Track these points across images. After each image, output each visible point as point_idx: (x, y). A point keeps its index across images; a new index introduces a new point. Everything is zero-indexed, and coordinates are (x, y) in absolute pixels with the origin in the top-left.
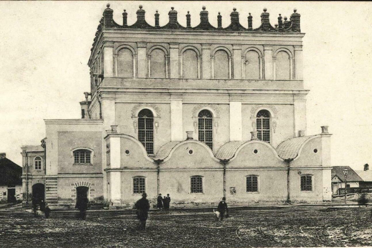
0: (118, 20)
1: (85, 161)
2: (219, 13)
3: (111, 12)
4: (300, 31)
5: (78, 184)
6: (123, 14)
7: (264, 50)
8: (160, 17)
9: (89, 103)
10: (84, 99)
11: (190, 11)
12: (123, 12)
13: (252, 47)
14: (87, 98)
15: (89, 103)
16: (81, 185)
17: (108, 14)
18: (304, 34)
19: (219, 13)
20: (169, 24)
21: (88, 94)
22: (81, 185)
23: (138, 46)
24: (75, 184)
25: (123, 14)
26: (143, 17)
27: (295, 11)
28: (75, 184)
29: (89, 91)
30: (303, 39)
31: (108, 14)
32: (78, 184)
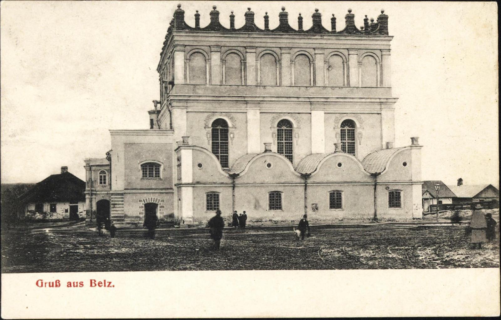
1: (154, 175)
4: (387, 33)
5: (147, 200)
6: (196, 15)
7: (349, 55)
9: (159, 112)
10: (153, 108)
11: (268, 12)
13: (336, 51)
14: (156, 106)
15: (159, 112)
16: (149, 201)
17: (179, 15)
18: (393, 37)
19: (300, 14)
21: (158, 103)
23: (212, 50)
24: (143, 200)
25: (196, 15)
27: (382, 12)
28: (143, 200)
29: (158, 99)
30: (391, 43)
31: (179, 15)
32: (147, 200)
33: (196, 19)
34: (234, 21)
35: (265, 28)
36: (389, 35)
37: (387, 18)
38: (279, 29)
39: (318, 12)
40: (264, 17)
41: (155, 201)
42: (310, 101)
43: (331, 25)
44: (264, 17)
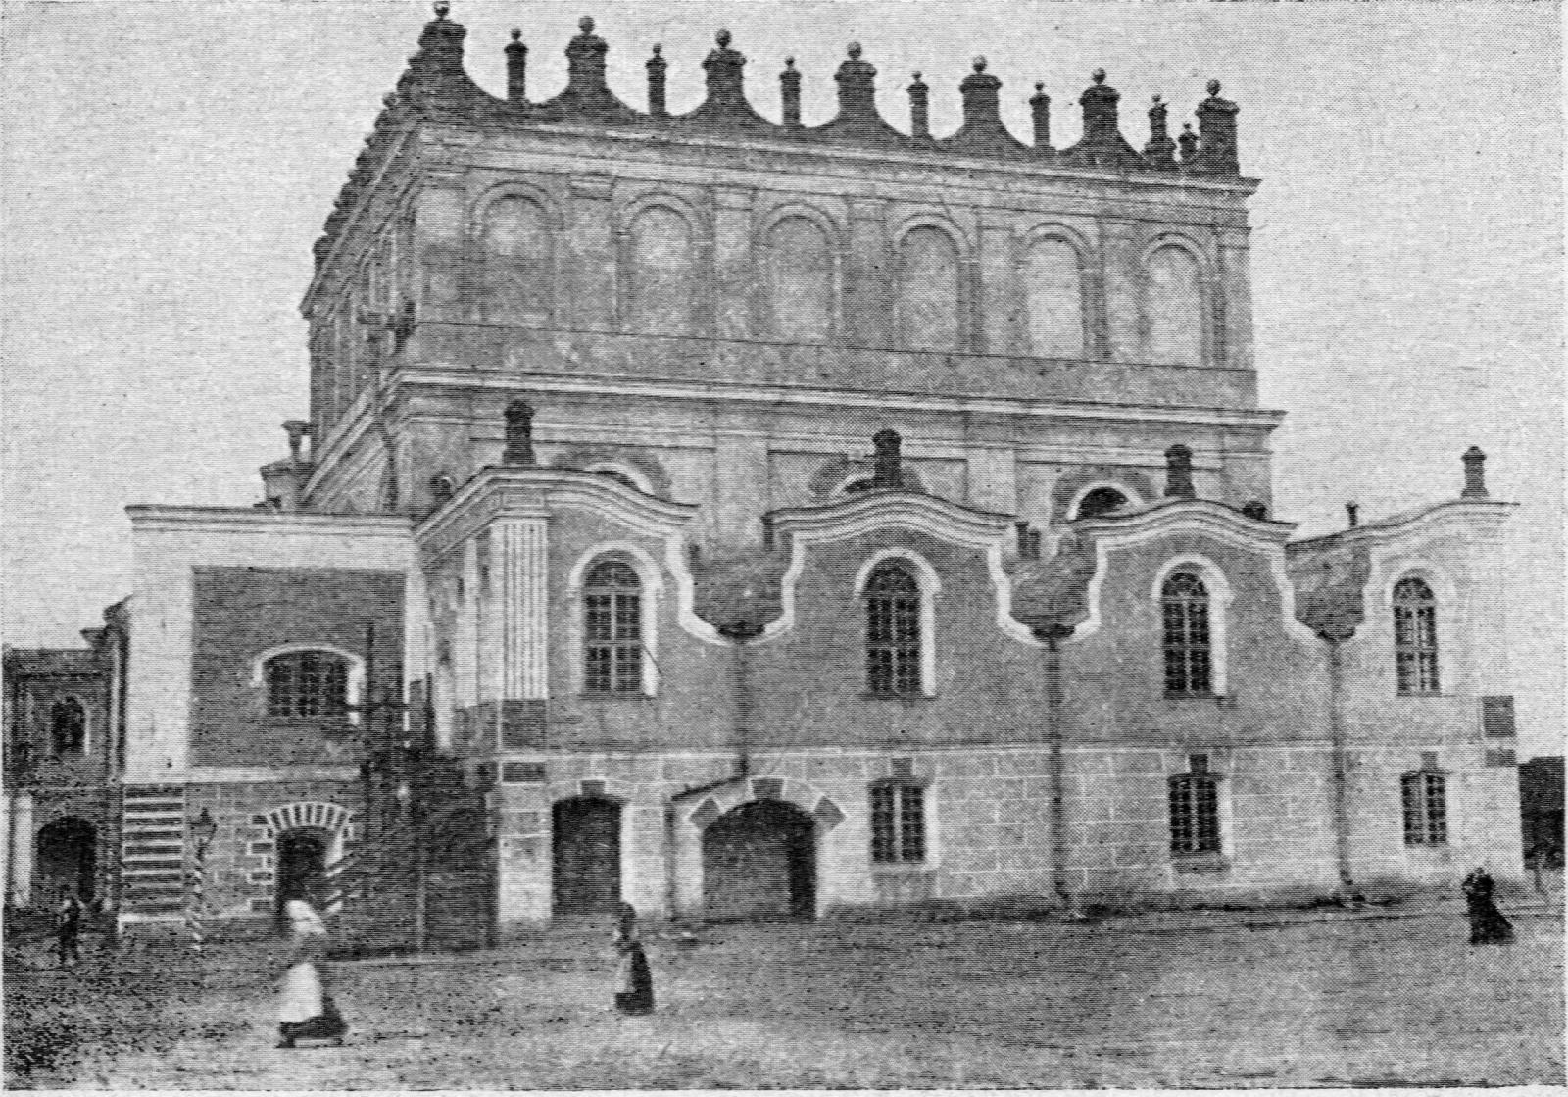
0: (486, 71)
1: (614, 681)
2: (516, 35)
3: (1112, 98)
4: (1235, 167)
5: (287, 818)
6: (784, 77)
7: (980, 229)
8: (671, 73)
9: (308, 469)
10: (282, 452)
11: (797, 57)
12: (784, 68)
13: (1053, 223)
14: (295, 445)
15: (308, 469)
16: (288, 823)
17: (443, 40)
18: (1256, 182)
19: (516, 35)
20: (568, 94)
21: (305, 429)
22: (288, 823)
23: (984, 223)
24: (269, 818)
25: (784, 77)
26: (1112, 118)
27: (979, 67)
28: (269, 818)
29: (306, 418)
30: (1248, 203)
31: (443, 40)
32: (287, 818)
33: (651, 79)
34: (914, 111)
35: (915, 128)
36: (1243, 172)
37: (873, 74)
38: (706, 115)
39: (1220, 95)
40: (508, 50)
41: (313, 817)
42: (962, 412)
43: (1241, 144)
44: (1032, 102)
